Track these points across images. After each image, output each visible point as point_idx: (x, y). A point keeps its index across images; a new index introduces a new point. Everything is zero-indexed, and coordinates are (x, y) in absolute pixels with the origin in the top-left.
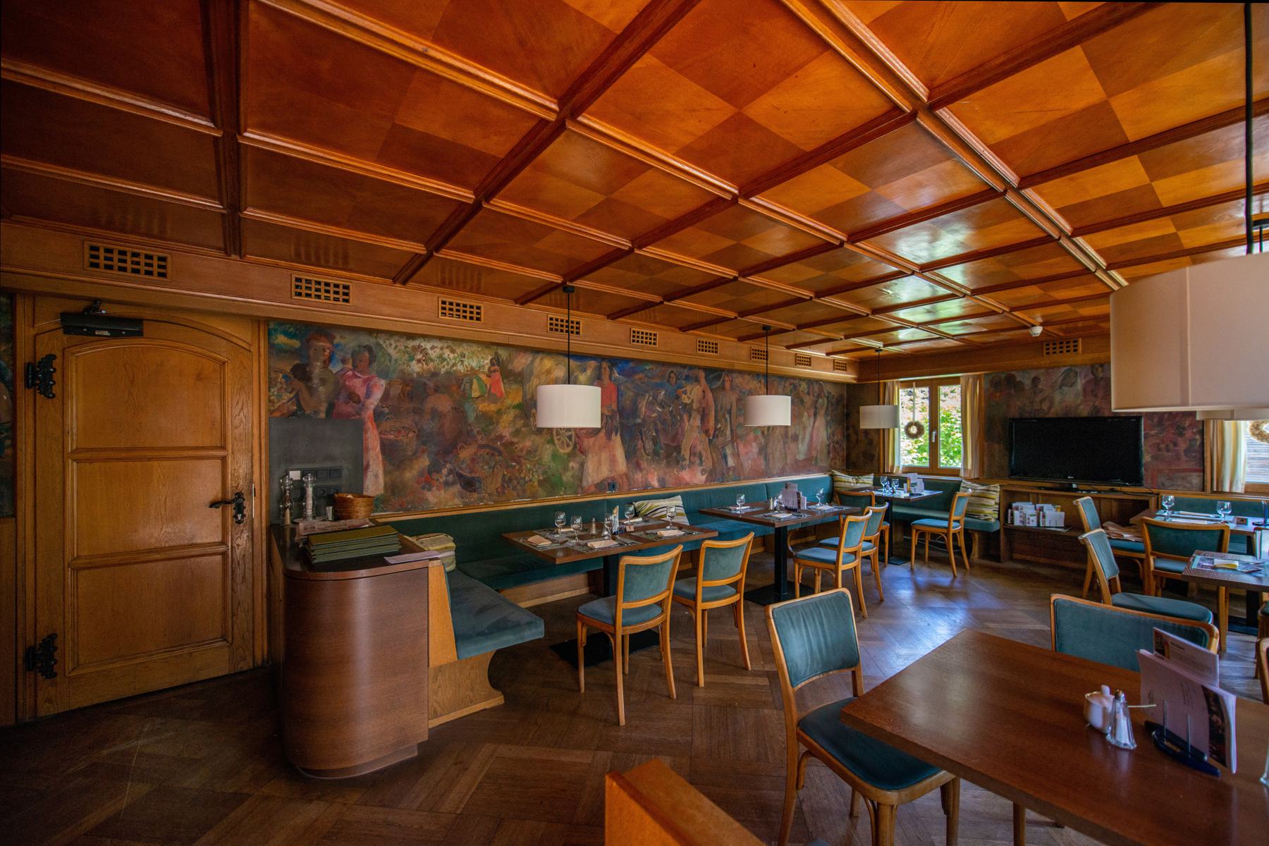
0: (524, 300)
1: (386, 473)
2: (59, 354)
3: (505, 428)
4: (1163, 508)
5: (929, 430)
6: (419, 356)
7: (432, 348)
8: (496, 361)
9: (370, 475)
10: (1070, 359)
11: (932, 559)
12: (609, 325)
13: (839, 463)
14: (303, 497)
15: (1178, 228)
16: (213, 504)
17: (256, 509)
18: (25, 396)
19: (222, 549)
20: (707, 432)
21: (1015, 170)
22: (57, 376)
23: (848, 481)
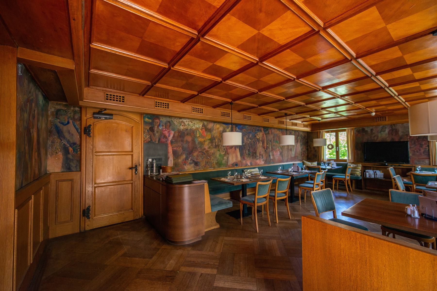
0: (215, 107)
1: (174, 160)
2: (92, 125)
3: (206, 146)
4: (417, 171)
5: (336, 146)
6: (183, 124)
7: (186, 121)
8: (204, 125)
9: (169, 160)
10: (384, 123)
11: (339, 189)
12: (238, 114)
13: (305, 158)
14: (152, 167)
15: (420, 84)
16: (130, 168)
17: (141, 170)
18: (84, 136)
19: (132, 182)
20: (264, 148)
21: (375, 71)
22: (92, 131)
23: (309, 164)
